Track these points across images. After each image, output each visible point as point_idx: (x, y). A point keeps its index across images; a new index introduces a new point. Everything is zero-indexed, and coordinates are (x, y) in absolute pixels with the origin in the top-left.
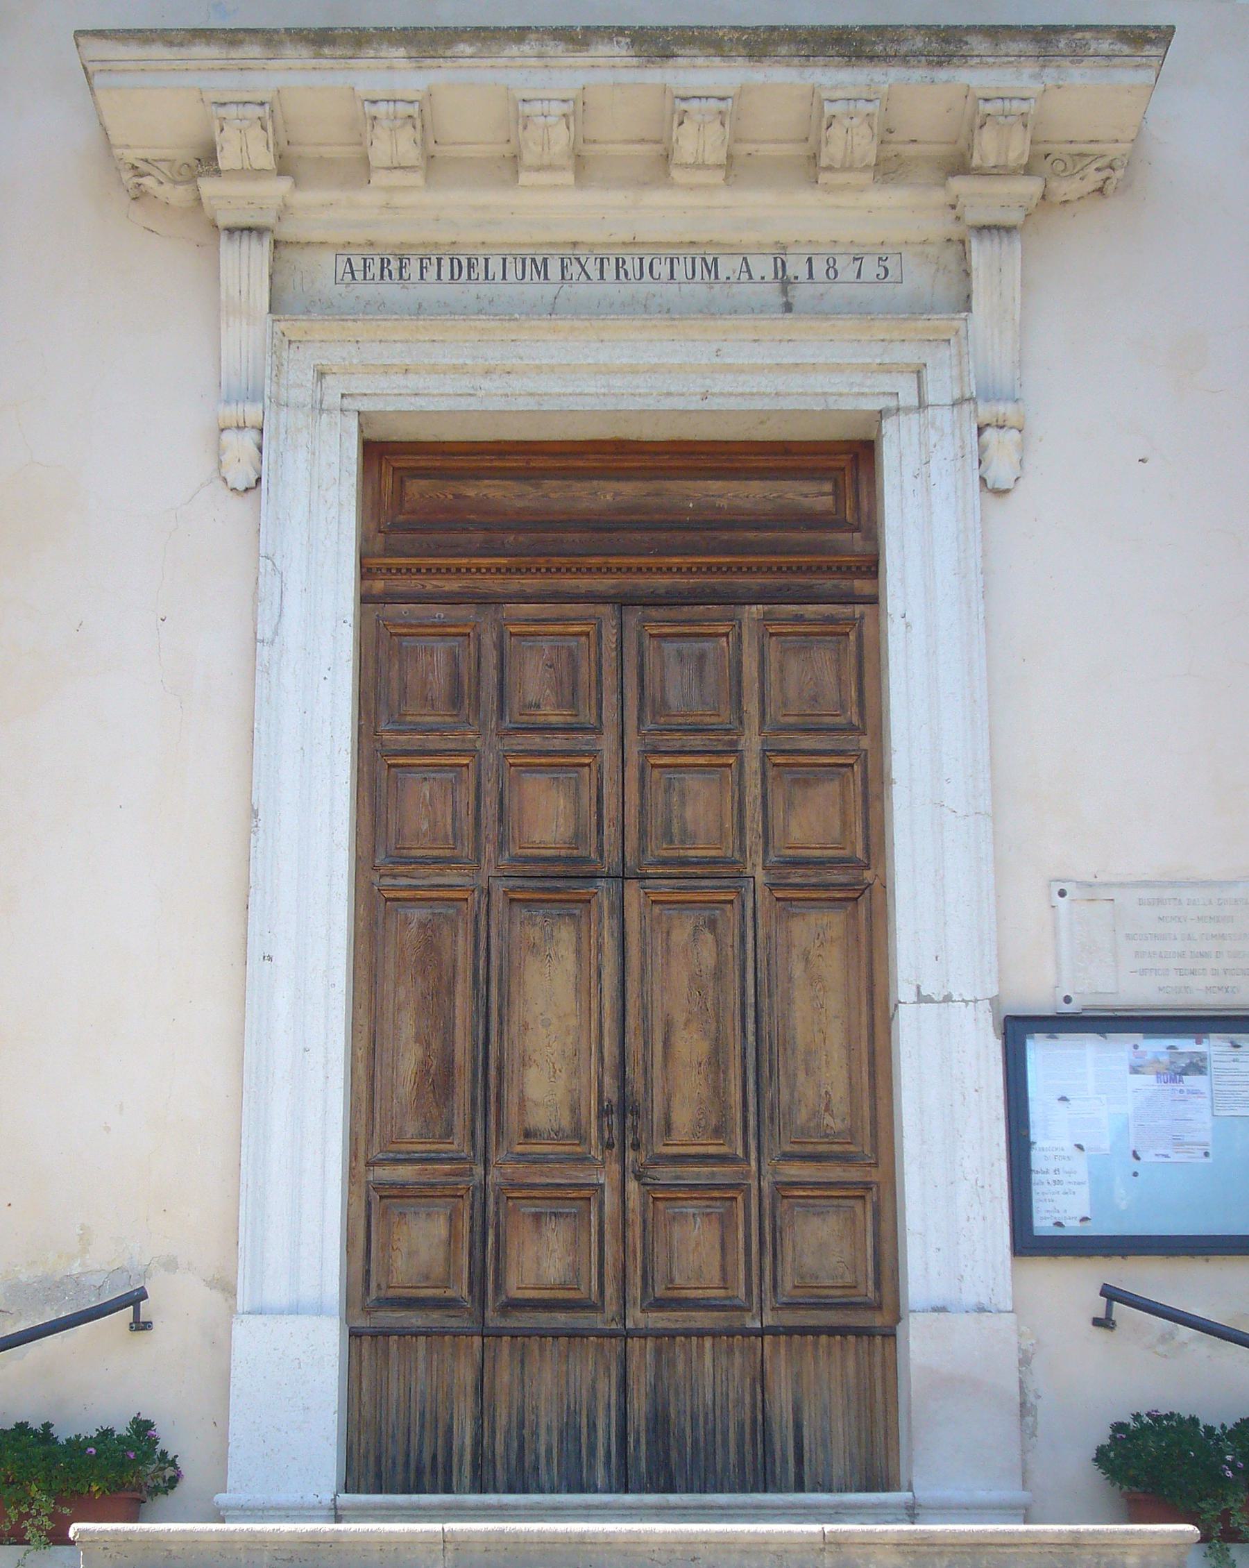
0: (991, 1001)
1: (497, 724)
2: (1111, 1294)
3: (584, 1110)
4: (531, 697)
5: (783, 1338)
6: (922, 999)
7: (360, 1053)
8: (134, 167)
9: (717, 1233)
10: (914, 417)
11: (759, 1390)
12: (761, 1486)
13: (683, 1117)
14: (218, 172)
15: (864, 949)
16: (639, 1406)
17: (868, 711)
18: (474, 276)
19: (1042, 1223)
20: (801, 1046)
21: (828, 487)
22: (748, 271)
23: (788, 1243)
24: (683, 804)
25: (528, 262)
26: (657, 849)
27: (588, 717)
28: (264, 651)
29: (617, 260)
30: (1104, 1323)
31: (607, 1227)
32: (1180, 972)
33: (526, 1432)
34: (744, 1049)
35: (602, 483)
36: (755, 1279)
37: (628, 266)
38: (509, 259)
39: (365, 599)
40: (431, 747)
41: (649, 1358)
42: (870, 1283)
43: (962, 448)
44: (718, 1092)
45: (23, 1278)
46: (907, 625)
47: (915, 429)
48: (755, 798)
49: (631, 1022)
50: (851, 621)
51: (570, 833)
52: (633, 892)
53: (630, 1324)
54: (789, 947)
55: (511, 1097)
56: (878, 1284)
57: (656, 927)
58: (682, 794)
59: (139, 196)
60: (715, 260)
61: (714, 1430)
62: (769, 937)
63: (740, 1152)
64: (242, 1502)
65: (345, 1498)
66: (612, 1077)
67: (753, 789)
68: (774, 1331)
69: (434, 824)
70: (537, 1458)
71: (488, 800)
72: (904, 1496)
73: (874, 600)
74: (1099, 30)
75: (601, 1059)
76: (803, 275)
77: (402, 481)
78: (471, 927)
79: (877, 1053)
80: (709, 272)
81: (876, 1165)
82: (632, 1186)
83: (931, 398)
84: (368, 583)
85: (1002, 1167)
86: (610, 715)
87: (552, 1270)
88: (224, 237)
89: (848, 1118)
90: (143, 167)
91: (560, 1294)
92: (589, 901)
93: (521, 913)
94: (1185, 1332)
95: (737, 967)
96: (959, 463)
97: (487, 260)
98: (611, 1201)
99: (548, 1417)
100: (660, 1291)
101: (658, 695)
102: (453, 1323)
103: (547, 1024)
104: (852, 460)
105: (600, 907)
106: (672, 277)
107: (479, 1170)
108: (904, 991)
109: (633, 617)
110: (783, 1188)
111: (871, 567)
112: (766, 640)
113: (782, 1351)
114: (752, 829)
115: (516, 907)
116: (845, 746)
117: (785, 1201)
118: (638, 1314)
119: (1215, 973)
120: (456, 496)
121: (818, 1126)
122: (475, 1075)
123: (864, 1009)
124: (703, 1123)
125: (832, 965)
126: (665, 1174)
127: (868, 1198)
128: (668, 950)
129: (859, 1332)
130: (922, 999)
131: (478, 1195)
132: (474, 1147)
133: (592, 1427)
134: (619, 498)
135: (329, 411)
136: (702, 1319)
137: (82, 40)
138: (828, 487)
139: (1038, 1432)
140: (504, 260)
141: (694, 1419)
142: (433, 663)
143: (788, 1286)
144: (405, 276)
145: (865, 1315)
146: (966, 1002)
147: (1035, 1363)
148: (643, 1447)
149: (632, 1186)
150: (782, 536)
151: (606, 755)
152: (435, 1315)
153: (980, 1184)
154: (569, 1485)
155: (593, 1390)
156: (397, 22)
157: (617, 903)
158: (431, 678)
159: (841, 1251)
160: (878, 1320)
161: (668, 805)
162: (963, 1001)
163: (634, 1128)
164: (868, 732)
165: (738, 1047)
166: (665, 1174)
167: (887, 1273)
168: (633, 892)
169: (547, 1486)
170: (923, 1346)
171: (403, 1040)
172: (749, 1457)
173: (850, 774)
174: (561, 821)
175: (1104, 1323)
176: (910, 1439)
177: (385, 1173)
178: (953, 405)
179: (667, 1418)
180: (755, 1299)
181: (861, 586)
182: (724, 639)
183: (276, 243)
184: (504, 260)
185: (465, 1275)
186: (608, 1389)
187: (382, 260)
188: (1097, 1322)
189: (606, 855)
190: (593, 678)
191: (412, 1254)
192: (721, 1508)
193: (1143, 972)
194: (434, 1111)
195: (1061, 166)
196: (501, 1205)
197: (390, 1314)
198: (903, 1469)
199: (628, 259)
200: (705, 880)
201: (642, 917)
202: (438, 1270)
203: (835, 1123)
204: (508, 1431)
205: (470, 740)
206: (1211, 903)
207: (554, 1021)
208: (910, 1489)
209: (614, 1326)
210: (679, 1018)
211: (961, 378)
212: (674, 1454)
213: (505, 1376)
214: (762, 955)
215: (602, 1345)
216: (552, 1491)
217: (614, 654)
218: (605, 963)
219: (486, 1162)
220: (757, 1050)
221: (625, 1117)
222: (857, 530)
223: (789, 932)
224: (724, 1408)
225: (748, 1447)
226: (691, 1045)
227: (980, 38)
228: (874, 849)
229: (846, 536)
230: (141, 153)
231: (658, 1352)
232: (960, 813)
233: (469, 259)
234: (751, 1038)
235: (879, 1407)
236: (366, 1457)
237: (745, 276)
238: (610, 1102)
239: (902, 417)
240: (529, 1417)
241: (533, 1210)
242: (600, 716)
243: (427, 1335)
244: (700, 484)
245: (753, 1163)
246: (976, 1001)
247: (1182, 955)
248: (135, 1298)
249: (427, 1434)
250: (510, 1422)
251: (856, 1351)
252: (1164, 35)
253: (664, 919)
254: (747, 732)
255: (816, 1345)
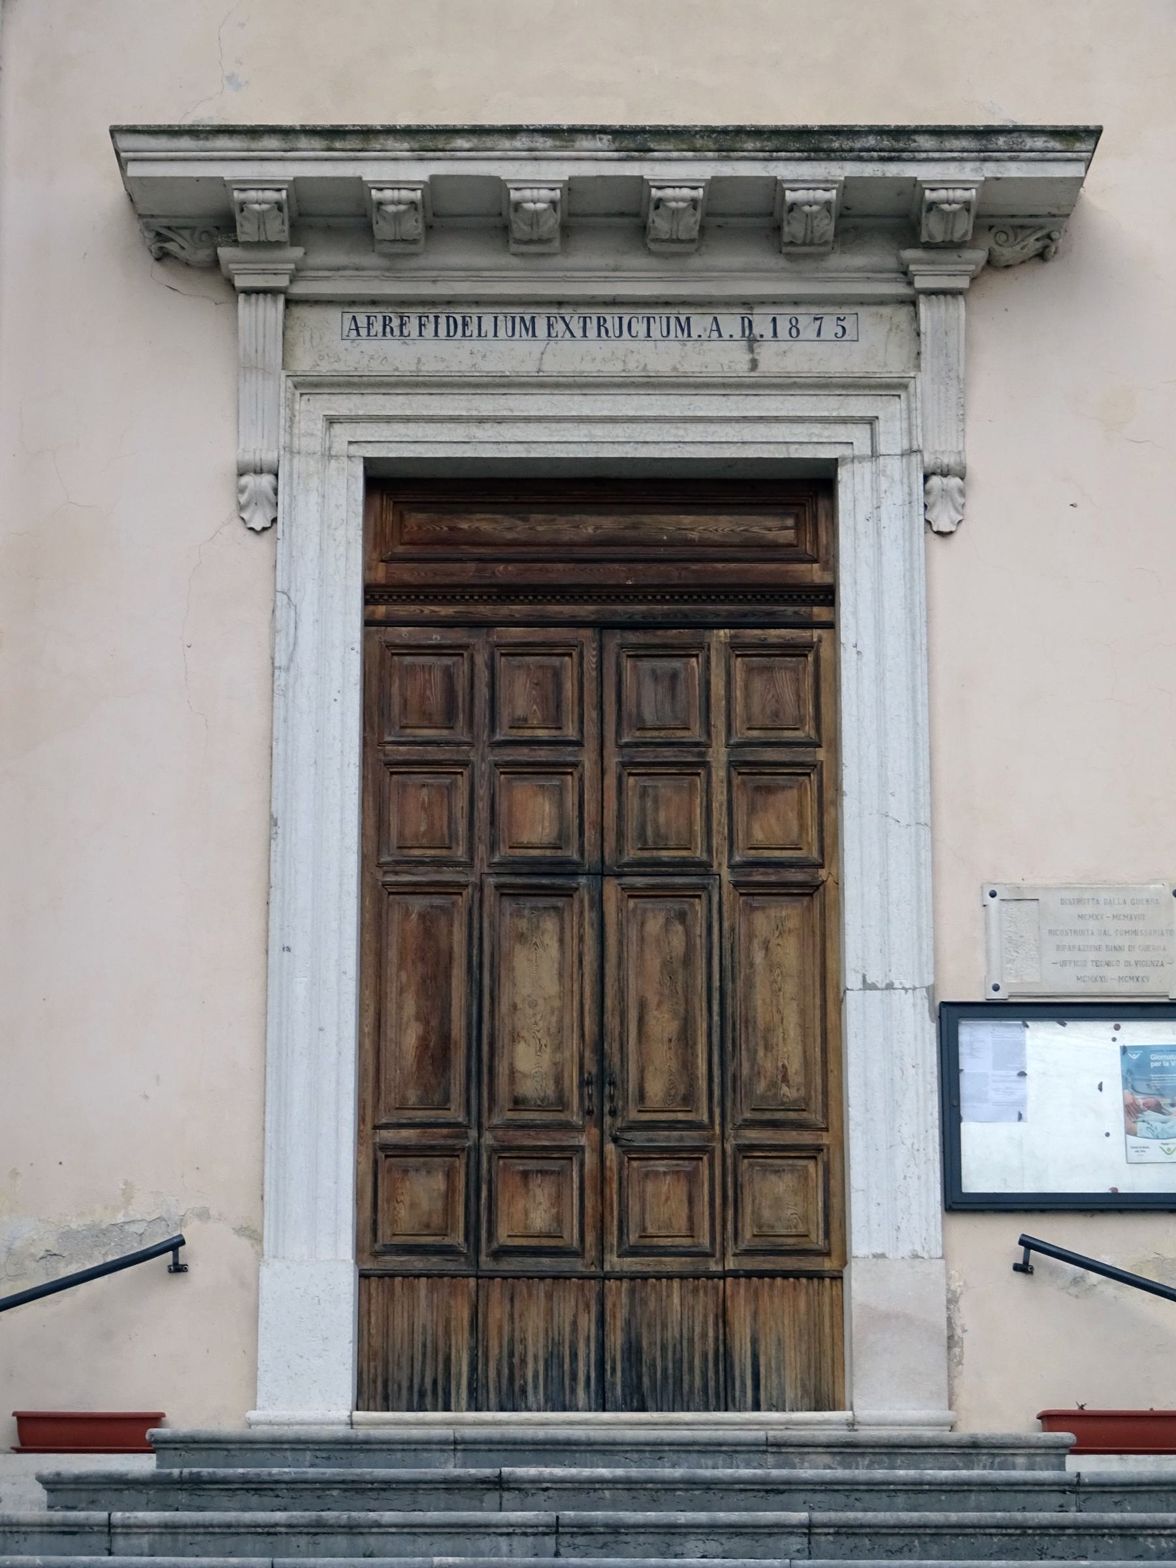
0: (928, 988)
1: (489, 736)
2: (1028, 1244)
3: (567, 1082)
4: (519, 712)
5: (743, 1280)
6: (867, 986)
7: (366, 1030)
8: (158, 234)
9: (685, 1189)
10: (867, 467)
11: (721, 1325)
12: (722, 1407)
13: (656, 1088)
14: (236, 241)
15: (818, 939)
16: (616, 1340)
17: (824, 726)
18: (468, 333)
19: (975, 1181)
20: (761, 1024)
21: (790, 522)
22: (718, 330)
23: (747, 1192)
24: (656, 810)
25: (518, 320)
26: (632, 853)
27: (570, 732)
28: (281, 677)
29: (599, 318)
30: (1023, 1268)
31: (587, 1183)
32: (1097, 964)
33: (516, 1360)
34: (710, 1028)
35: (584, 517)
36: (718, 1228)
37: (609, 325)
38: (501, 318)
39: (369, 623)
40: (429, 757)
41: (624, 1299)
42: (821, 1233)
43: (910, 494)
44: (687, 1065)
45: (74, 1226)
46: (858, 653)
47: (868, 477)
48: (721, 805)
49: (609, 1002)
50: (810, 646)
51: (555, 834)
52: (611, 889)
53: (607, 1268)
54: (751, 936)
55: (502, 1069)
56: (827, 1235)
57: (631, 918)
58: (656, 800)
59: (162, 256)
60: (688, 319)
61: (681, 1359)
62: (733, 929)
63: (705, 1118)
64: (271, 1418)
65: (359, 1415)
66: (592, 1052)
67: (720, 796)
68: (735, 1275)
69: (431, 826)
70: (526, 1383)
71: (481, 805)
72: (847, 1414)
73: (831, 625)
74: (1034, 131)
75: (582, 1036)
76: (768, 334)
77: (402, 516)
78: (465, 919)
79: (829, 1031)
80: (683, 330)
81: (827, 1129)
82: (610, 1147)
83: (882, 449)
84: (371, 608)
85: (935, 1133)
86: (590, 729)
87: (539, 1220)
88: (242, 297)
89: (803, 1088)
90: (164, 232)
91: (545, 1242)
92: (571, 896)
93: (508, 905)
94: (1094, 1277)
95: (704, 955)
96: (907, 509)
97: (480, 318)
98: (590, 1159)
99: (535, 1347)
100: (633, 1238)
101: (634, 710)
102: (451, 1266)
103: (533, 1005)
104: (806, 490)
105: (582, 901)
106: (649, 335)
107: (473, 1133)
108: (852, 980)
109: (614, 639)
110: (745, 1150)
111: (828, 595)
112: (732, 660)
113: (742, 1291)
114: (719, 832)
115: (504, 899)
116: (799, 759)
117: (746, 1161)
118: (615, 1259)
119: (1128, 964)
120: (451, 529)
121: (776, 1095)
122: (469, 1049)
123: (818, 993)
124: (673, 1092)
125: (789, 951)
126: (639, 1138)
127: (819, 1159)
128: (642, 940)
129: (811, 1275)
130: (867, 986)
131: (473, 1154)
132: (468, 1113)
133: (574, 1356)
134: (599, 531)
135: (337, 457)
136: (672, 1264)
137: (117, 136)
138: (790, 522)
139: (964, 1361)
140: (496, 318)
141: (664, 1348)
142: (427, 680)
143: (748, 1235)
144: (406, 332)
145: (813, 1262)
146: (906, 990)
147: (962, 1303)
148: (619, 1373)
149: (610, 1147)
150: (739, 558)
151: (587, 765)
152: (435, 1259)
153: (916, 1147)
154: (554, 1404)
155: (574, 1324)
156: (402, 121)
157: (597, 897)
158: (428, 693)
159: (795, 1205)
160: (828, 1265)
161: (643, 810)
162: (903, 988)
163: (612, 1098)
164: (824, 744)
165: (705, 1026)
166: (639, 1138)
167: (835, 1225)
168: (611, 889)
169: (535, 1407)
170: (862, 1288)
171: (405, 1018)
172: (712, 1384)
173: (807, 781)
174: (547, 824)
175: (1023, 1268)
176: (851, 1366)
177: (388, 1136)
178: (902, 455)
179: (639, 1351)
180: (718, 1247)
181: (820, 613)
182: (694, 660)
183: (288, 303)
184: (496, 318)
185: (462, 1225)
186: (587, 1324)
187: (385, 317)
188: (1017, 1268)
189: (586, 854)
190: (576, 694)
191: (413, 1206)
192: (687, 1424)
193: (1064, 964)
194: (433, 1081)
195: (1003, 237)
196: (494, 1164)
197: (395, 1258)
198: (847, 1395)
199: (608, 318)
200: (675, 879)
201: (619, 910)
202: (437, 1220)
203: (788, 1093)
204: (500, 1360)
205: (464, 751)
206: (1125, 902)
207: (540, 1001)
208: (852, 1409)
209: (593, 1269)
210: (652, 1000)
211: (910, 432)
212: (646, 1380)
213: (497, 1313)
214: (727, 945)
215: (583, 1285)
216: (538, 1410)
217: (594, 660)
218: (586, 950)
219: (480, 1126)
220: (724, 1023)
221: (603, 1087)
222: (816, 561)
223: (750, 923)
224: (691, 1341)
225: (711, 1374)
226: (662, 1024)
227: (927, 137)
228: (828, 850)
229: (803, 567)
230: (165, 222)
231: (632, 1292)
232: (903, 823)
233: (464, 318)
234: (716, 1018)
235: (828, 1341)
236: (375, 1382)
237: (715, 335)
238: (590, 1074)
239: (856, 464)
240: (519, 1349)
241: (521, 1168)
242: (581, 731)
243: (428, 1276)
244: (674, 518)
245: (717, 1128)
246: (914, 989)
247: (1098, 948)
248: (175, 1245)
249: (429, 1361)
250: (501, 1352)
251: (807, 1293)
252: (1095, 134)
253: (639, 912)
254: (714, 744)
255: (771, 1287)
